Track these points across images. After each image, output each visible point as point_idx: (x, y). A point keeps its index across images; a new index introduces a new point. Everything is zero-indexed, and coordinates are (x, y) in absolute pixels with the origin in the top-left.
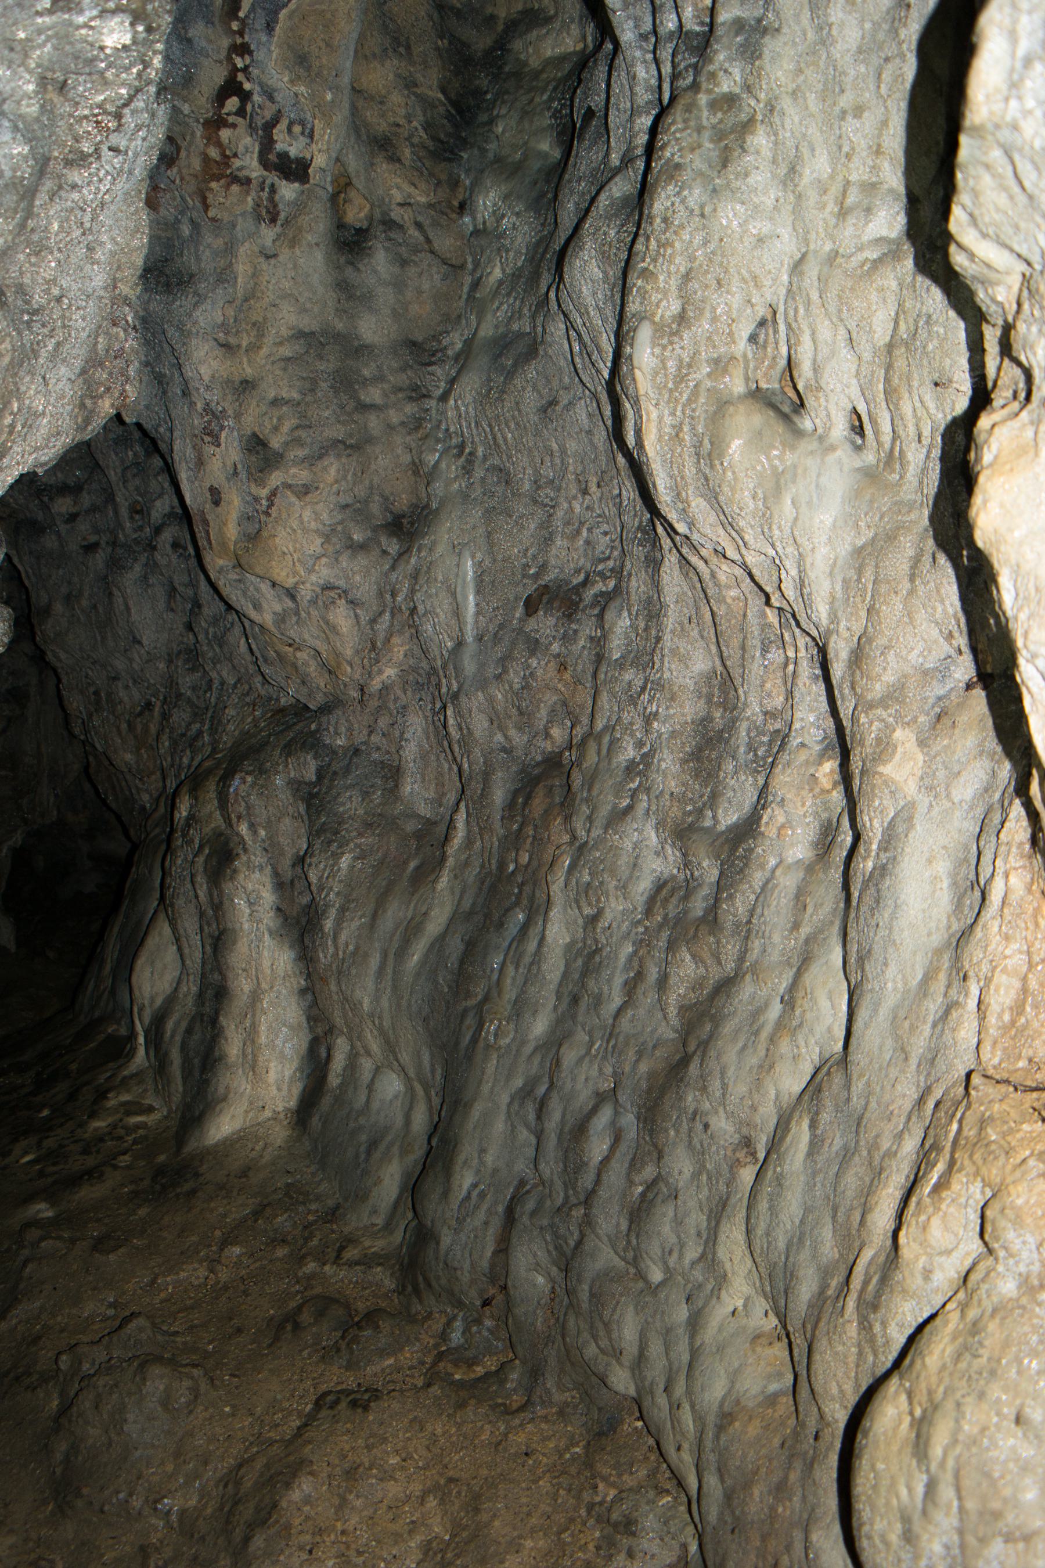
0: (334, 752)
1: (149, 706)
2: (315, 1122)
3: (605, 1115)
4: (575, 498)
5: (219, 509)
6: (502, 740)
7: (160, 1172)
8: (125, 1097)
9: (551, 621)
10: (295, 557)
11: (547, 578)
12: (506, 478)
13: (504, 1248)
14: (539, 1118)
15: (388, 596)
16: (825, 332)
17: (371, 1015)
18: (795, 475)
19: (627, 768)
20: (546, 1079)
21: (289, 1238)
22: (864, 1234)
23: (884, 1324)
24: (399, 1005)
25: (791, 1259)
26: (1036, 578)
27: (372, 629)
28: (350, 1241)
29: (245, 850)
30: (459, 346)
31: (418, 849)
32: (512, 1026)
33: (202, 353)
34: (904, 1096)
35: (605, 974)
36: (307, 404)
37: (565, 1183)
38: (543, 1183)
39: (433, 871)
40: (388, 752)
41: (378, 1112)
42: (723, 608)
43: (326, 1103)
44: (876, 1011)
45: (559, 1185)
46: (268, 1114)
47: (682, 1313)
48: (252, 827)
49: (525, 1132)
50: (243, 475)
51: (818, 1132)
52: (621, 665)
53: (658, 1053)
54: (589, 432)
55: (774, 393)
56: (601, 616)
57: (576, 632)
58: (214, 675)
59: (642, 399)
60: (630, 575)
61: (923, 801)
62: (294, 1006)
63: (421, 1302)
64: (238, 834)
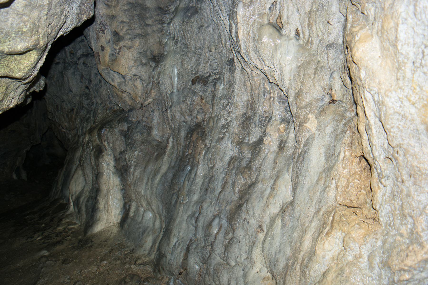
0: (132, 122)
1: (73, 110)
2: (126, 226)
3: (217, 221)
4: (207, 52)
5: (104, 52)
6: (184, 119)
7: (80, 241)
8: (68, 220)
9: (200, 86)
10: (126, 66)
11: (198, 74)
12: (187, 46)
13: (186, 258)
14: (196, 222)
15: (151, 78)
16: (291, 8)
17: (144, 196)
18: (281, 46)
19: (222, 126)
20: (198, 212)
21: (120, 258)
22: (301, 248)
23: (309, 271)
24: (152, 193)
25: (277, 256)
26: (372, 70)
27: (147, 88)
28: (138, 259)
29: (106, 150)
30: (173, 9)
31: (157, 149)
32: (187, 198)
33: (101, 7)
34: (311, 211)
35: (216, 183)
36: (131, 23)
37: (205, 240)
38: (197, 240)
39: (162, 155)
40: (148, 123)
41: (145, 223)
42: (254, 83)
43: (129, 220)
44: (302, 189)
45: (203, 241)
46: (112, 224)
47: (241, 273)
48: (108, 143)
49: (192, 226)
50: (112, 42)
51: (285, 222)
52: (221, 98)
53: (232, 204)
54: (213, 34)
55: (275, 24)
56: (215, 85)
57: (207, 89)
58: (94, 101)
59: (239, 23)
60: (224, 74)
61: (317, 133)
62: (119, 194)
63: (160, 274)
64: (104, 145)
